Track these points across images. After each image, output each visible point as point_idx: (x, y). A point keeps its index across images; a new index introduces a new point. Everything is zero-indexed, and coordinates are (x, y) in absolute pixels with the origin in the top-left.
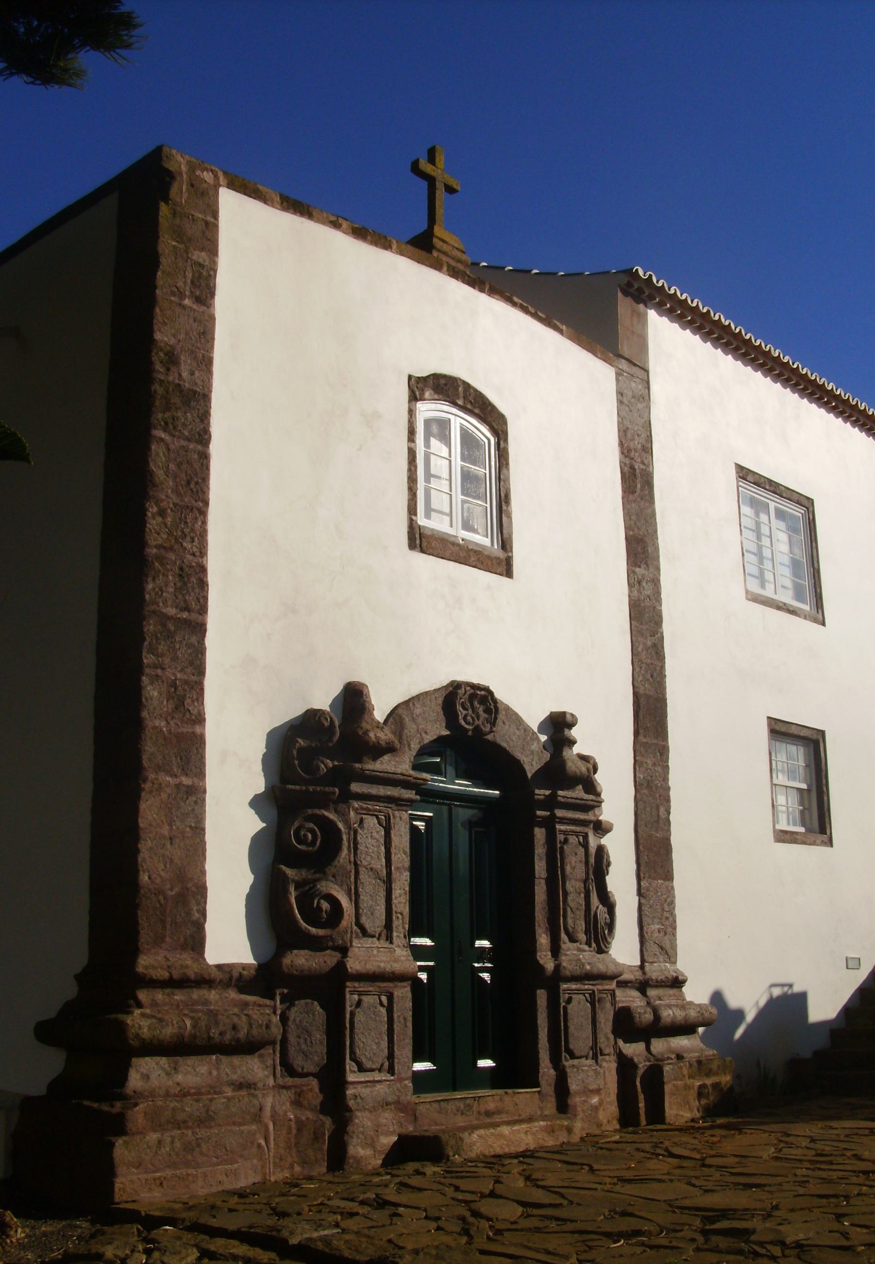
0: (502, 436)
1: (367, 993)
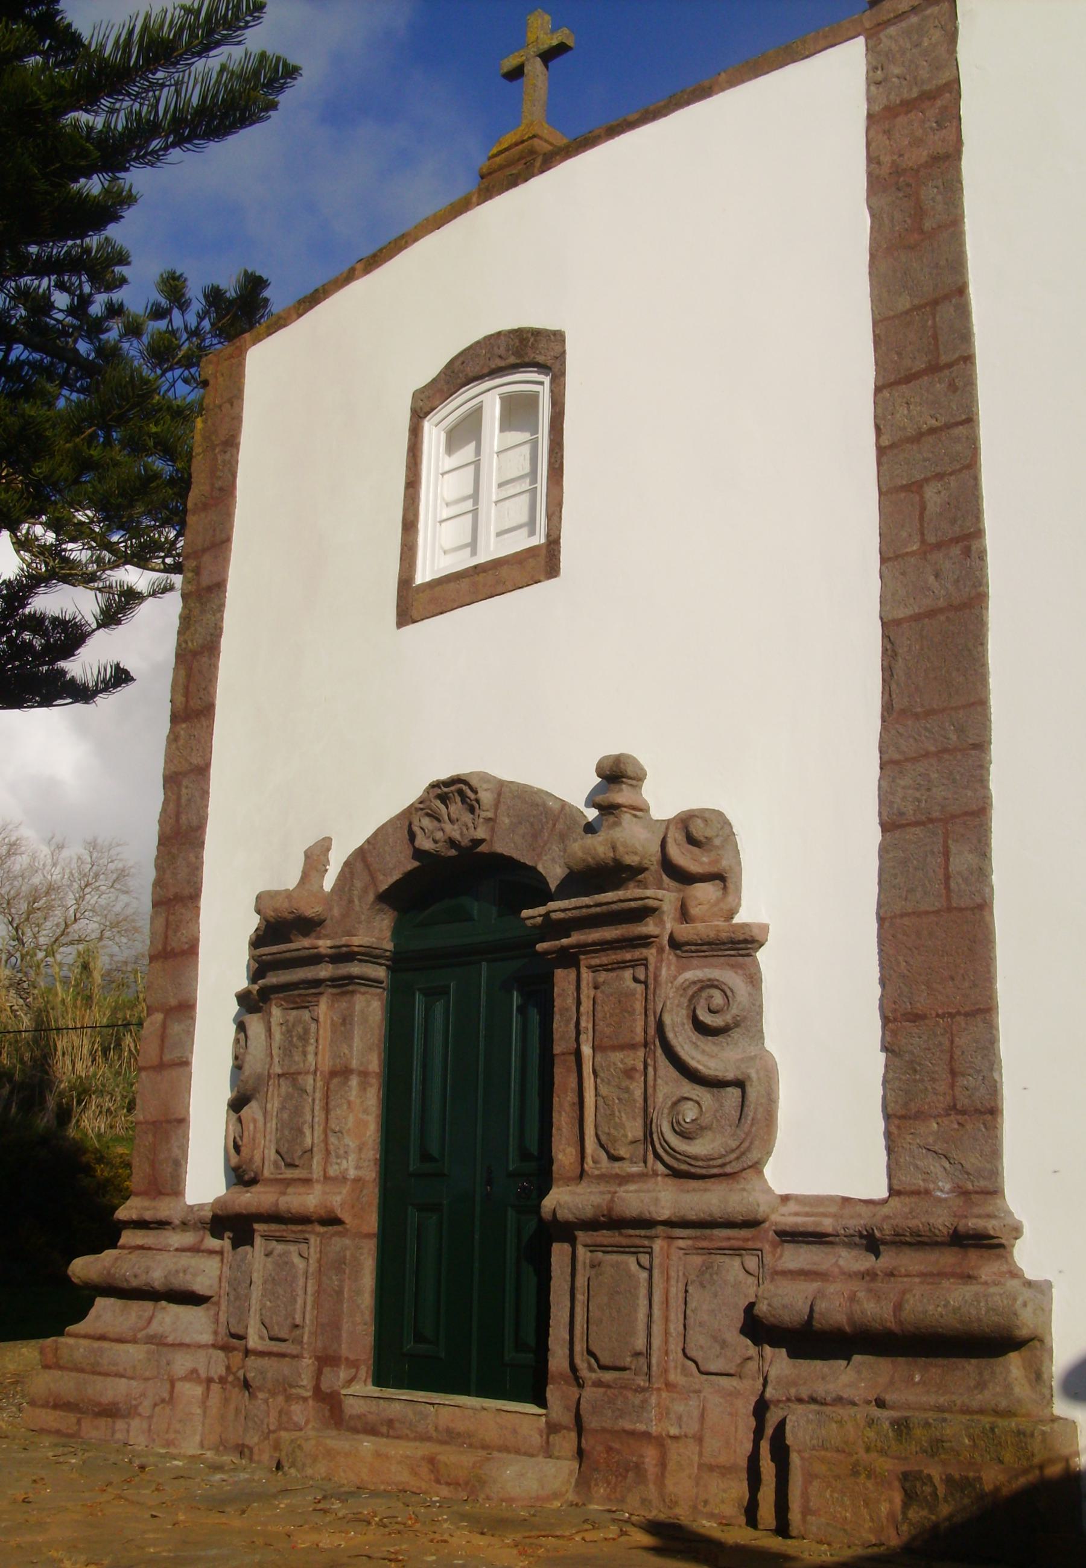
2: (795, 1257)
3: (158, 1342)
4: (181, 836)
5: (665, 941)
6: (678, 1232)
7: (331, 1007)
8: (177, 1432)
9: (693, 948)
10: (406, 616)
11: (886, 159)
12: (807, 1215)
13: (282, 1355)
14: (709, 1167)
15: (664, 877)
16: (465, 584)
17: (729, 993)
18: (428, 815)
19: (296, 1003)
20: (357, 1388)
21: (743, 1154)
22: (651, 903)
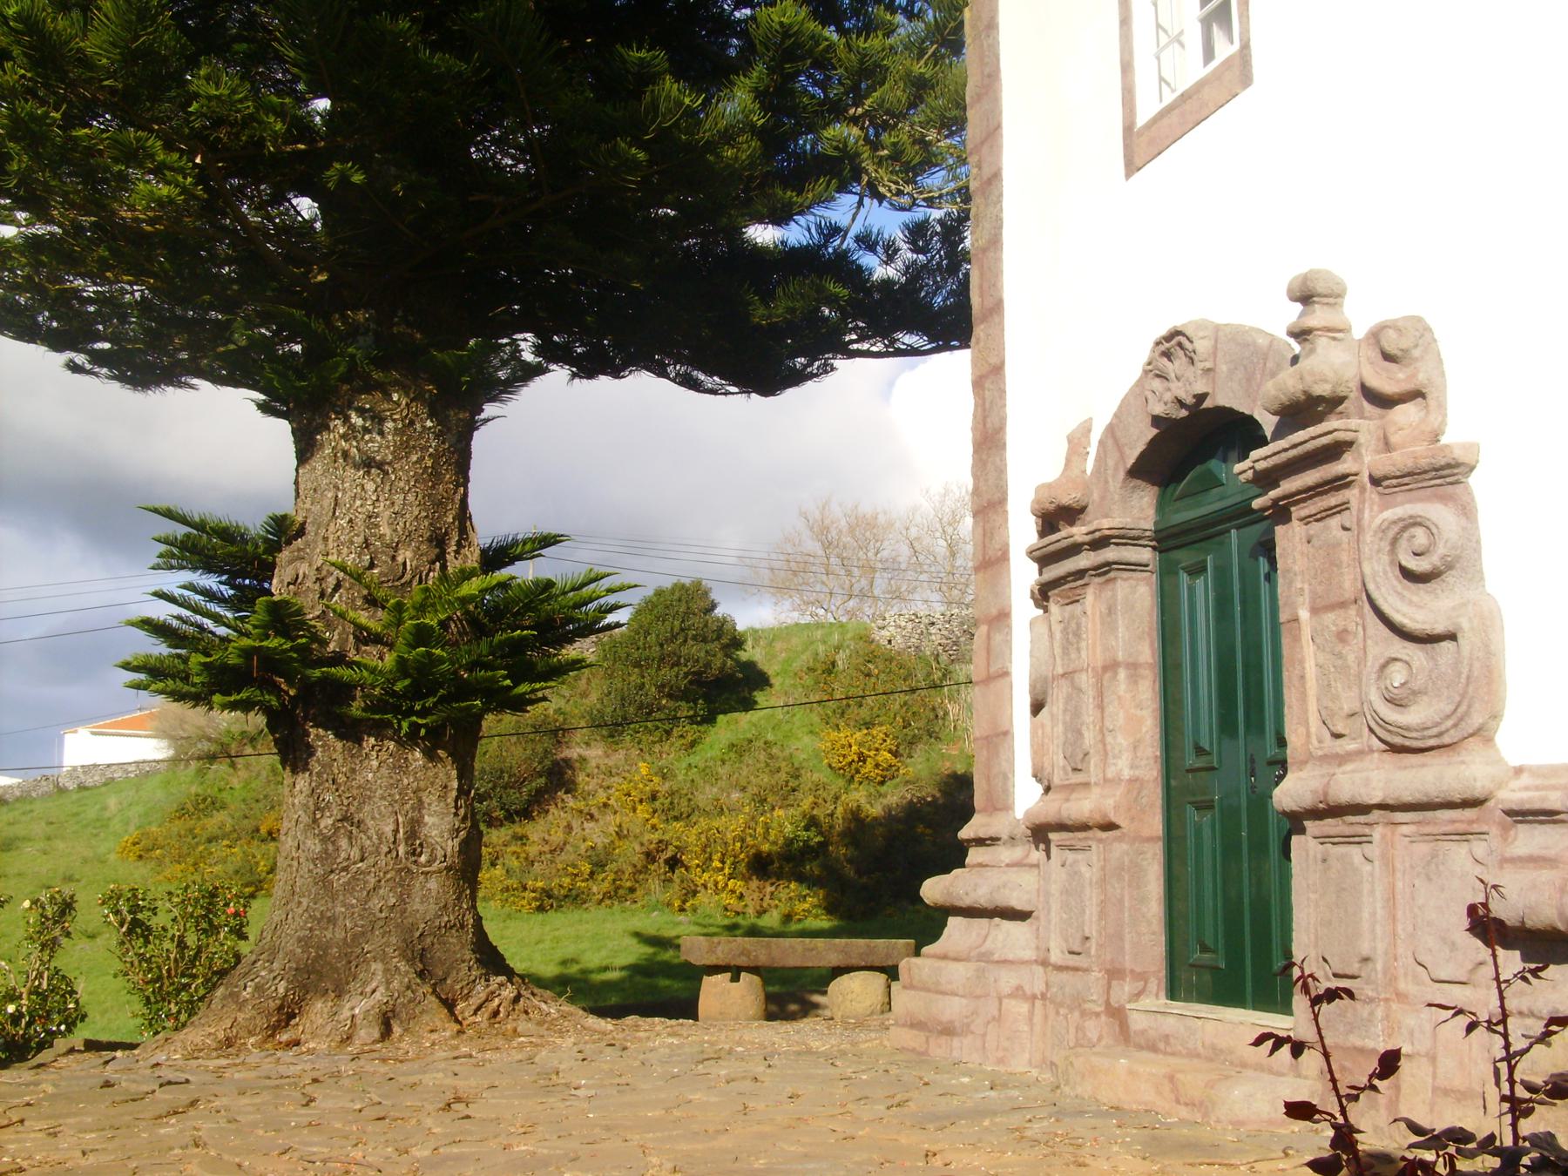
2: (1529, 839)
3: (985, 958)
4: (989, 441)
5: (1366, 480)
6: (1400, 816)
7: (1097, 597)
8: (1005, 1049)
9: (1394, 482)
10: (1132, 167)
12: (1537, 788)
13: (1076, 969)
14: (1424, 738)
15: (1365, 404)
16: (1174, 117)
17: (1434, 530)
18: (1158, 376)
20: (1147, 1002)
21: (1461, 719)
22: (1341, 436)
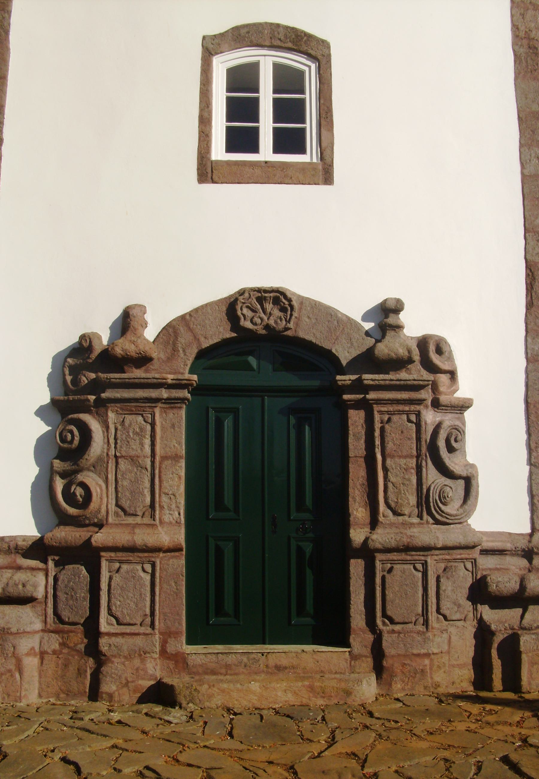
0: (323, 62)
1: (128, 562)
11: (522, 28)
19: (132, 411)
